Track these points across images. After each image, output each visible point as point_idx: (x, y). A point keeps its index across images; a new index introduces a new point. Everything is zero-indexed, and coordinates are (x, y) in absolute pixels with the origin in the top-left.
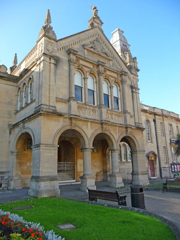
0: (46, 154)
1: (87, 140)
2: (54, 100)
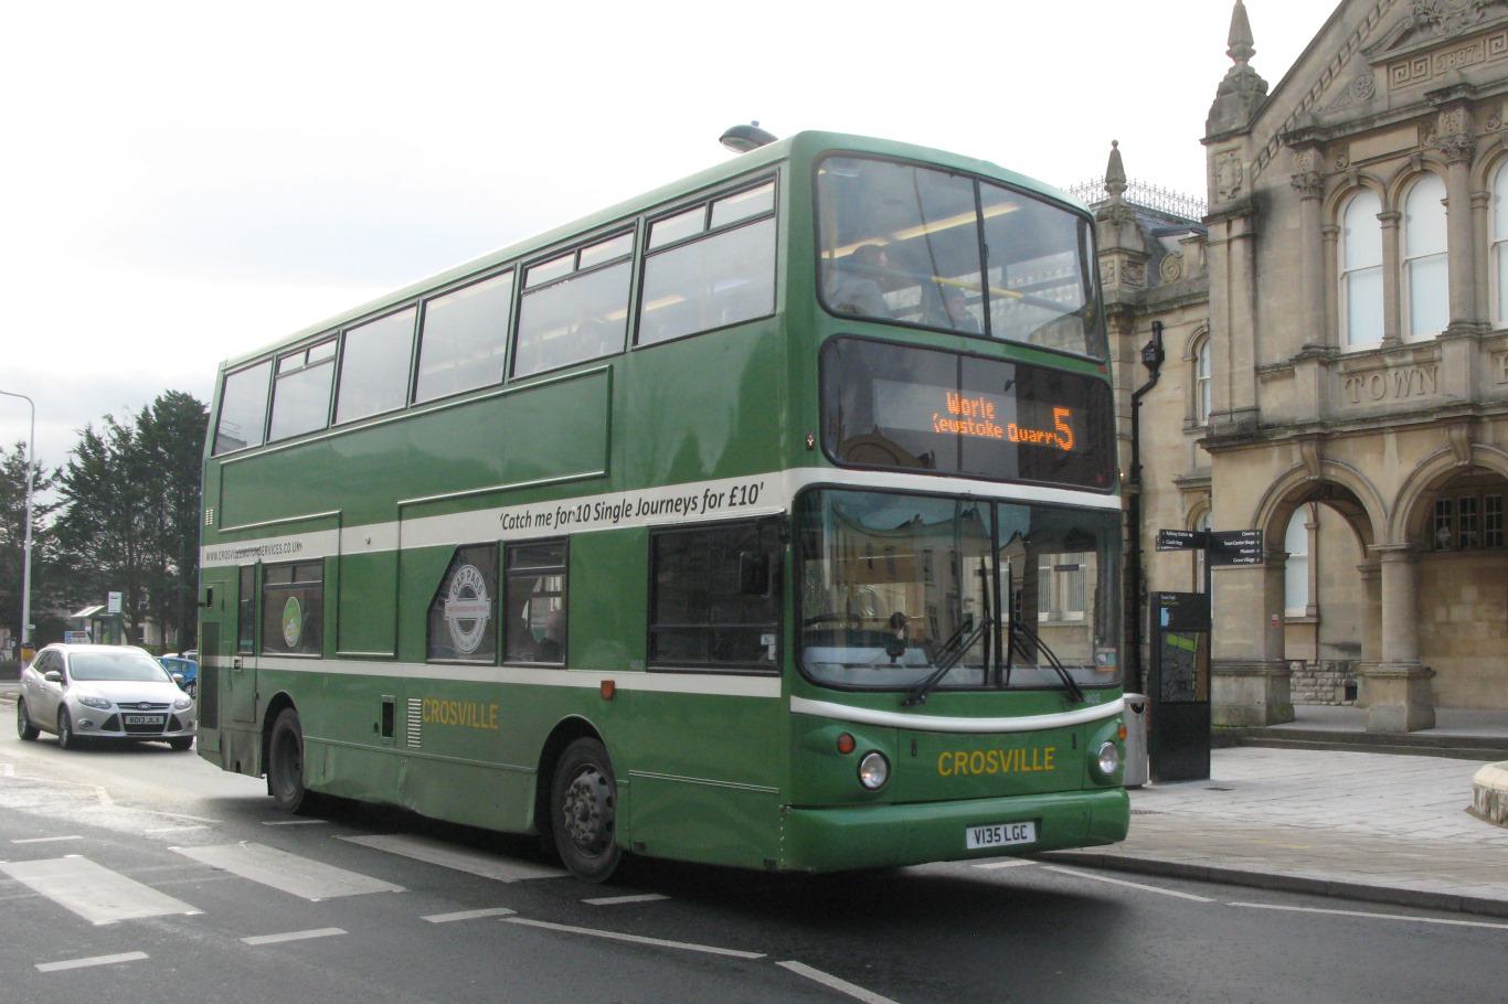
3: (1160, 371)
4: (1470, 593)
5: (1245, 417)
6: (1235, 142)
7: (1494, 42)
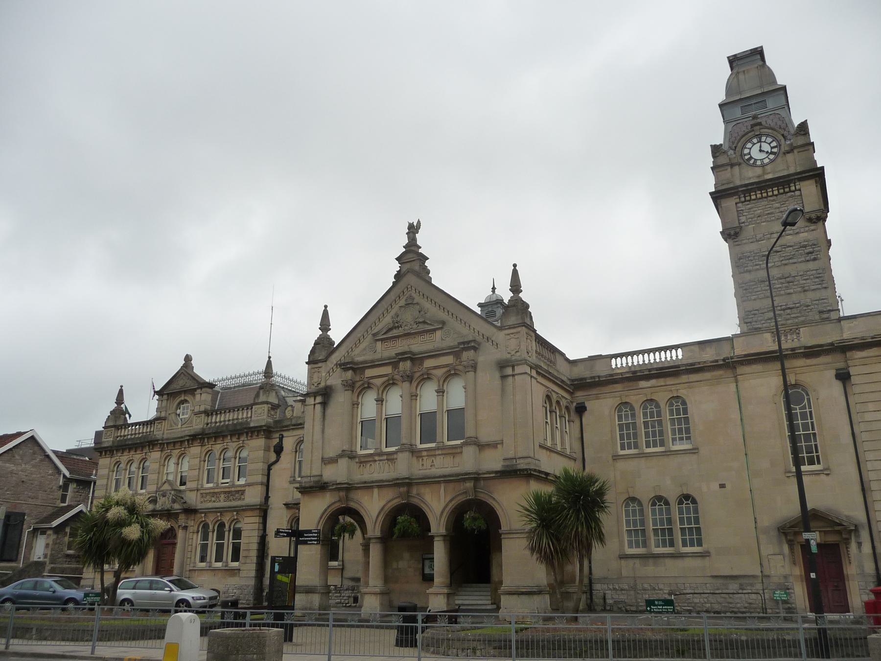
4: (406, 555)
5: (316, 479)
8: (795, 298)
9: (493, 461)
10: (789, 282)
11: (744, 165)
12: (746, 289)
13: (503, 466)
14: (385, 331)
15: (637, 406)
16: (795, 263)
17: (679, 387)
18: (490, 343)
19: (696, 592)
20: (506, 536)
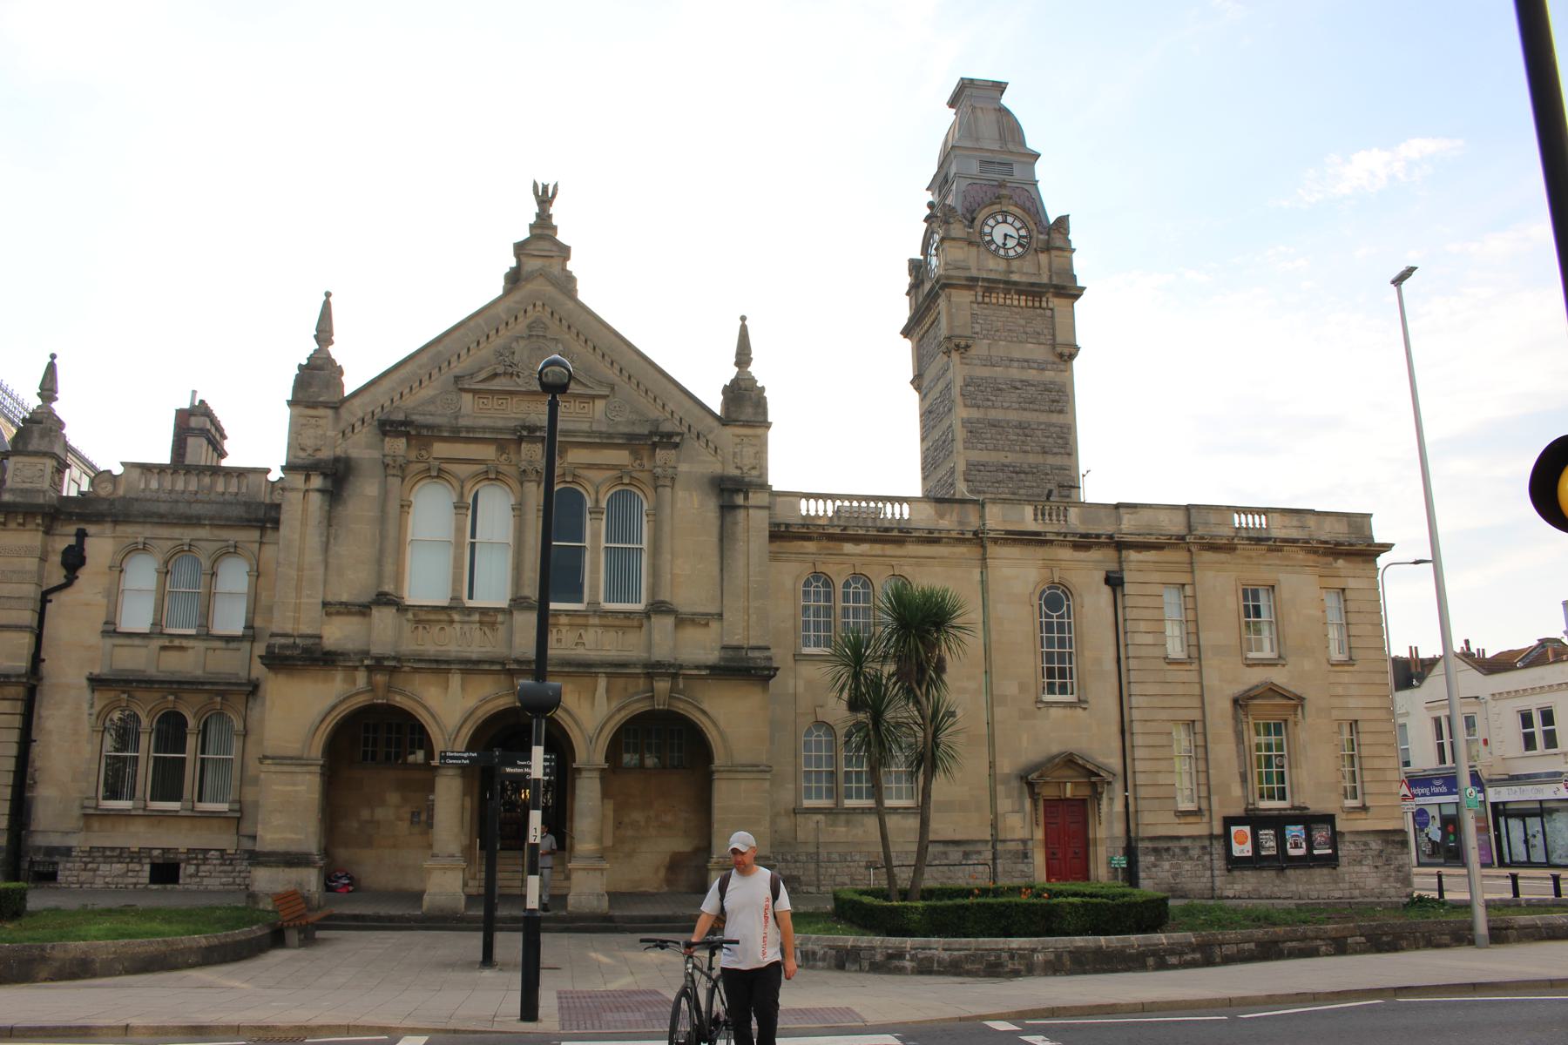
0: (280, 788)
1: (440, 737)
2: (318, 611)
3: (78, 574)
4: (393, 798)
5: (310, 642)
6: (321, 412)
7: (482, 400)
8: (1032, 459)
9: (700, 647)
10: (1026, 436)
11: (982, 249)
12: (971, 432)
13: (721, 659)
14: (483, 375)
15: (839, 583)
16: (1036, 410)
17: (903, 561)
18: (702, 442)
19: (905, 863)
20: (725, 775)
